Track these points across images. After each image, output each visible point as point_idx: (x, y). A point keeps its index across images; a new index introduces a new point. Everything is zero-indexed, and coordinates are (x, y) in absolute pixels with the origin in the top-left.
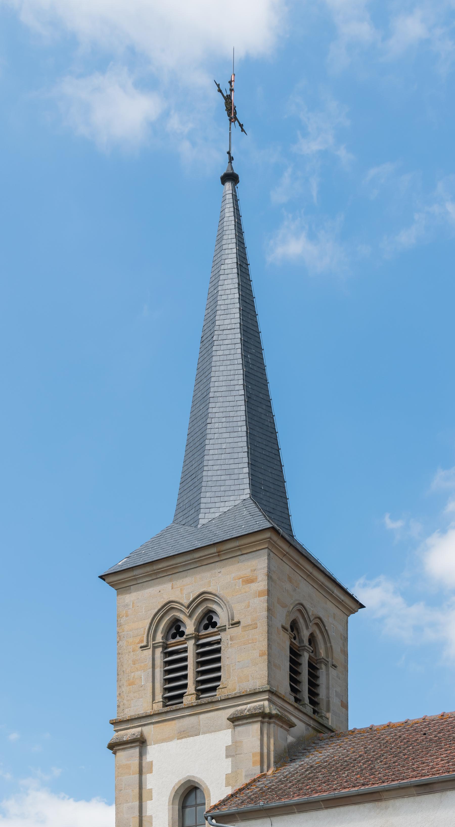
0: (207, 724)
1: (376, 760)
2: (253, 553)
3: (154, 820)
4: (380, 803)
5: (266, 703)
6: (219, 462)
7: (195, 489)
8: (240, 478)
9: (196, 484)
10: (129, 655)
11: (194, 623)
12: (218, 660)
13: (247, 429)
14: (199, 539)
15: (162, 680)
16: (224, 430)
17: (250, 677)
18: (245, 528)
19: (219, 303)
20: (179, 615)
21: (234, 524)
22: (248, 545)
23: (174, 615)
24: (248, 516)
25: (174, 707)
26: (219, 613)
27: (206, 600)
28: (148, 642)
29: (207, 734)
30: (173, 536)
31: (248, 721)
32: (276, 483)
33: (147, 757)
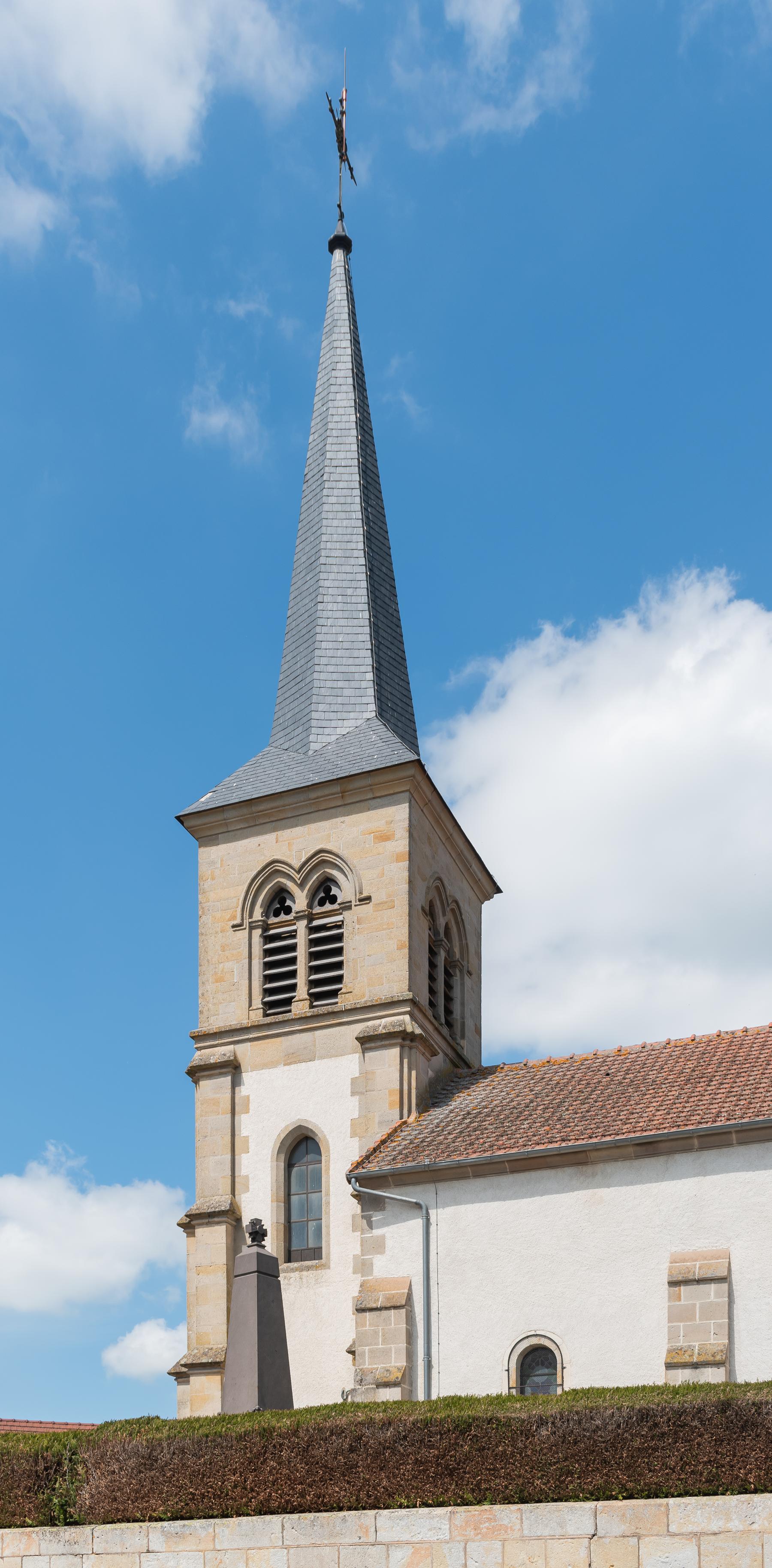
0: (325, 1045)
1: (558, 1107)
2: (389, 797)
3: (251, 1182)
4: (584, 1168)
5: (407, 1018)
6: (333, 661)
7: (303, 699)
8: (363, 687)
9: (304, 690)
10: (215, 937)
11: (307, 896)
12: (339, 951)
13: (370, 616)
14: (314, 772)
15: (262, 977)
16: (339, 614)
17: (385, 978)
18: (379, 759)
19: (330, 426)
20: (285, 883)
21: (362, 753)
22: (383, 785)
23: (278, 882)
24: (378, 742)
25: (280, 1018)
26: (342, 882)
27: (324, 862)
28: (242, 919)
29: (325, 1060)
30: (274, 764)
31: (383, 1043)
32: (404, 701)
33: (242, 1090)
